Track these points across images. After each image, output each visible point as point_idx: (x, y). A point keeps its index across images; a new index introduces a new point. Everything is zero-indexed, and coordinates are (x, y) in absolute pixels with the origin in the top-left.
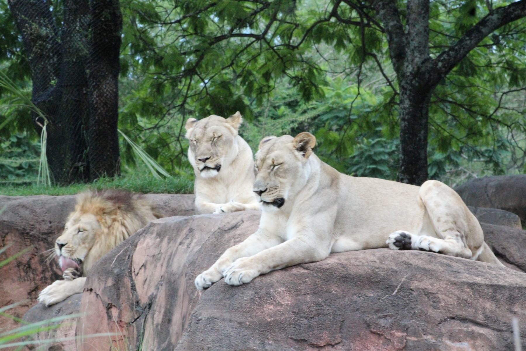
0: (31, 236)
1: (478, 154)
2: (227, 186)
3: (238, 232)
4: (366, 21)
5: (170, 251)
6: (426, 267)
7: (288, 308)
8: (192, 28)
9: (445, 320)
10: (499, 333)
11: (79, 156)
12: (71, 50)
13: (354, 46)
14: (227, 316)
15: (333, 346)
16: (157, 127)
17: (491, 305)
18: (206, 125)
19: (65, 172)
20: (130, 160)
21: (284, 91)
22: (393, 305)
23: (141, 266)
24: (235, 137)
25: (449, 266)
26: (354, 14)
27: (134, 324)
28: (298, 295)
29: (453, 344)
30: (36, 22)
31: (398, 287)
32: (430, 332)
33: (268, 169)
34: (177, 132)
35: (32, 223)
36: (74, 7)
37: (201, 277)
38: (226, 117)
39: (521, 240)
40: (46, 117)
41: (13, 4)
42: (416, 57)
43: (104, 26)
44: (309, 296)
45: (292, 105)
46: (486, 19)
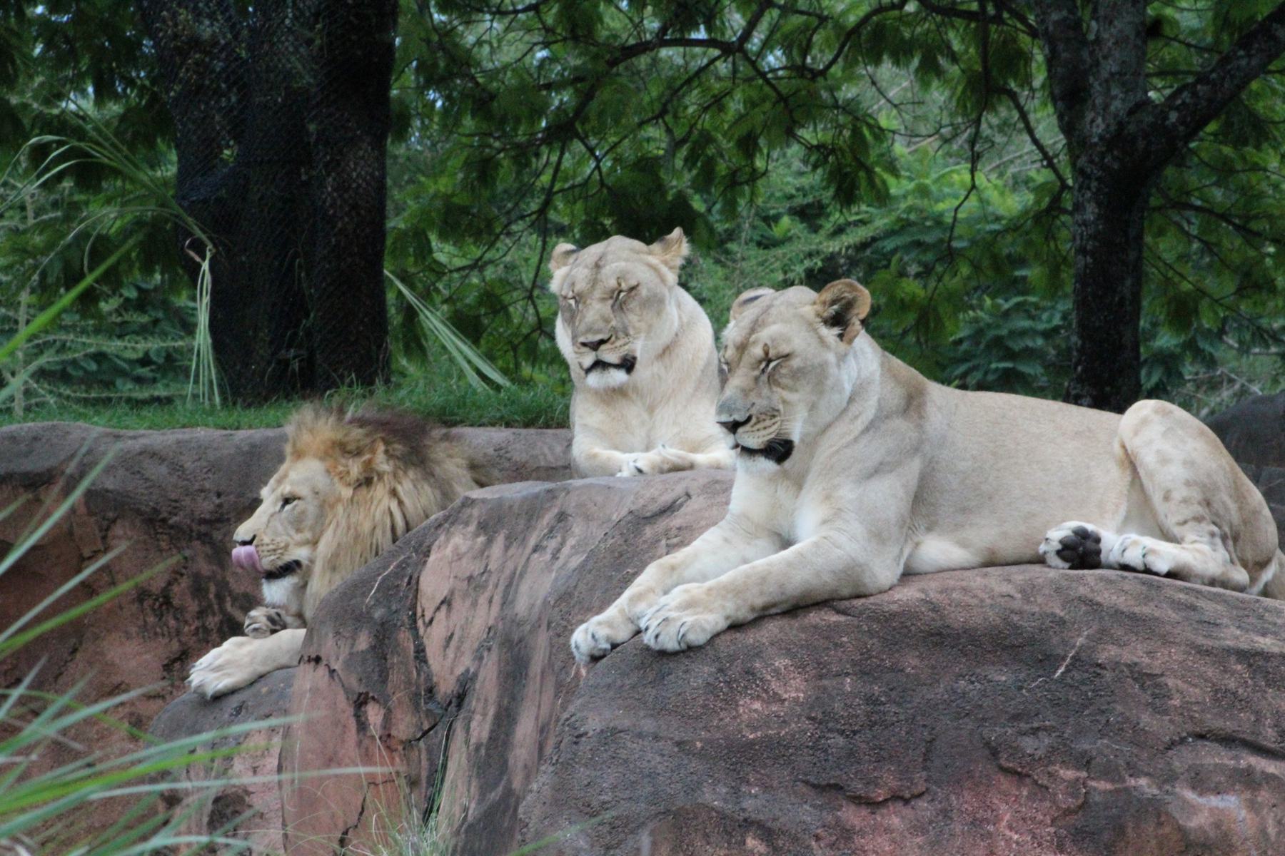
0: (172, 527)
2: (651, 410)
3: (676, 521)
5: (510, 565)
6: (1137, 610)
7: (798, 709)
9: (1183, 741)
12: (272, 75)
14: (648, 725)
15: (906, 802)
16: (478, 265)
18: (600, 259)
20: (413, 345)
21: (789, 179)
22: (1055, 703)
24: (670, 289)
25: (1193, 608)
27: (422, 743)
28: (821, 677)
29: (1201, 800)
30: (186, 8)
33: (754, 369)
34: (527, 277)
35: (173, 496)
37: (586, 631)
38: (648, 242)
40: (211, 239)
42: (1115, 97)
43: (352, 18)
45: (809, 214)
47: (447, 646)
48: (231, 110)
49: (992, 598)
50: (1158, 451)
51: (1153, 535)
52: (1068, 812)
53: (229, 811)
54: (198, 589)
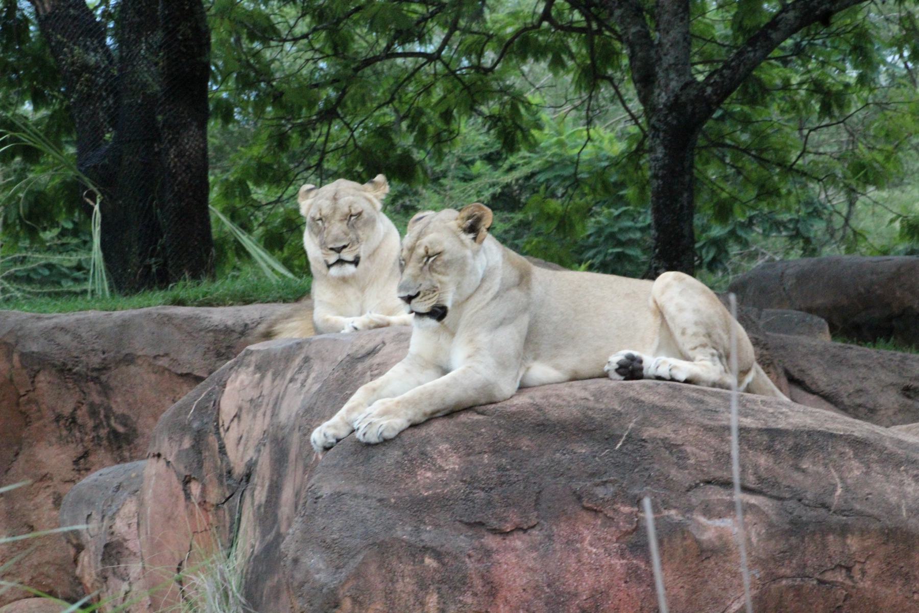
0: (75, 374)
1: (778, 225)
2: (363, 290)
3: (377, 359)
4: (594, 26)
5: (276, 391)
6: (666, 404)
7: (455, 475)
8: (330, 47)
9: (697, 485)
10: (779, 503)
11: (151, 248)
12: (134, 86)
13: (579, 65)
14: (360, 489)
15: (525, 531)
17: (766, 461)
19: (130, 274)
20: (242, 253)
22: (616, 465)
23: (232, 417)
25: (702, 402)
26: (577, 16)
27: (225, 506)
28: (469, 455)
29: (710, 522)
30: (79, 45)
31: (624, 438)
32: (674, 504)
33: (420, 262)
35: (75, 354)
36: (137, 19)
37: (320, 431)
38: (362, 182)
39: (828, 357)
40: (99, 190)
41: (43, 18)
42: (672, 79)
43: (182, 48)
44: (486, 456)
45: (492, 159)
46: (778, 19)
47: (238, 444)
48: (109, 109)
49: (576, 400)
50: (677, 304)
51: (675, 356)
52: (627, 533)
53: (114, 552)
54: (93, 413)
